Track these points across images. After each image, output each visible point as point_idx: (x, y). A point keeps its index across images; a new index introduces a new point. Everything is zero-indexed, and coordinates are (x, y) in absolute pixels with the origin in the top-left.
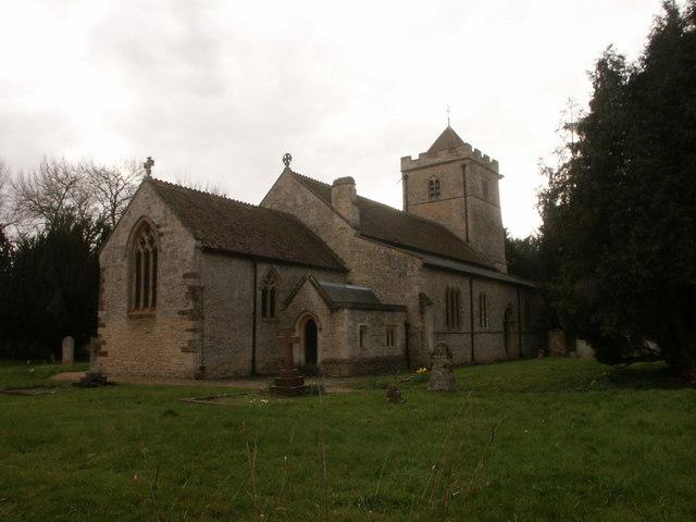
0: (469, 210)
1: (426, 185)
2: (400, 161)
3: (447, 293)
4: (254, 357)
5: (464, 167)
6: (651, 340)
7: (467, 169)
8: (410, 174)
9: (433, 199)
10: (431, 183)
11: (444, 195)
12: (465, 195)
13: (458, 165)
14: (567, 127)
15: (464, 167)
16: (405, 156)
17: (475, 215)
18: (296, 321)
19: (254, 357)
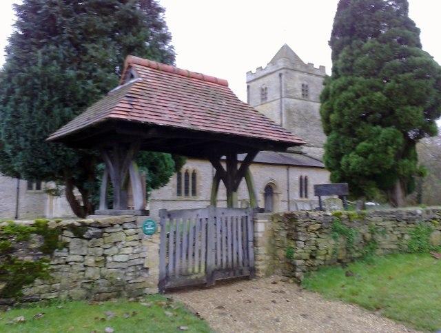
0: (283, 109)
1: (259, 92)
2: (246, 75)
3: (299, 144)
4: (18, 185)
5: (280, 75)
6: (236, 166)
7: (283, 77)
8: (250, 84)
9: (264, 102)
10: (263, 90)
11: (269, 99)
12: (281, 97)
13: (277, 74)
14: (13, 25)
15: (280, 75)
16: (322, 65)
17: (285, 105)
18: (285, 157)
19: (18, 185)
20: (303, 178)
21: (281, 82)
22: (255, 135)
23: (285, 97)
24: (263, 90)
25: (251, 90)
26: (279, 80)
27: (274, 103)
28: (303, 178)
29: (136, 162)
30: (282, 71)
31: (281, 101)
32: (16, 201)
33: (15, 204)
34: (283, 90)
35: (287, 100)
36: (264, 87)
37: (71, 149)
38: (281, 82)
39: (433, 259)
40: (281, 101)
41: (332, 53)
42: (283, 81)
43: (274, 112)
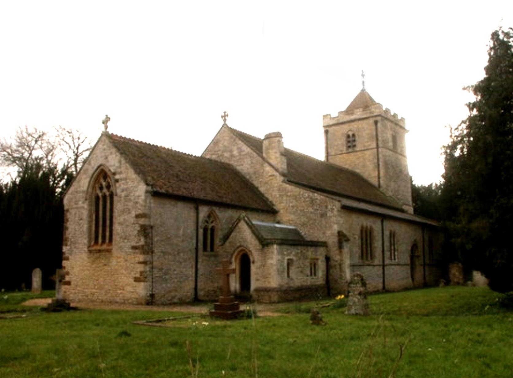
5: (376, 123)
7: (379, 125)
9: (350, 150)
10: (348, 136)
12: (377, 147)
13: (371, 121)
15: (376, 123)
20: (393, 232)
21: (376, 129)
22: (97, 171)
23: (382, 147)
24: (348, 136)
25: (330, 135)
26: (374, 127)
27: (367, 153)
28: (393, 232)
29: (20, 157)
30: (379, 118)
31: (378, 151)
32: (194, 267)
33: (194, 270)
34: (380, 138)
35: (384, 150)
36: (350, 133)
37: (465, 150)
38: (376, 129)
39: (371, 268)
40: (378, 151)
41: (260, 139)
42: (379, 130)
43: (368, 163)
